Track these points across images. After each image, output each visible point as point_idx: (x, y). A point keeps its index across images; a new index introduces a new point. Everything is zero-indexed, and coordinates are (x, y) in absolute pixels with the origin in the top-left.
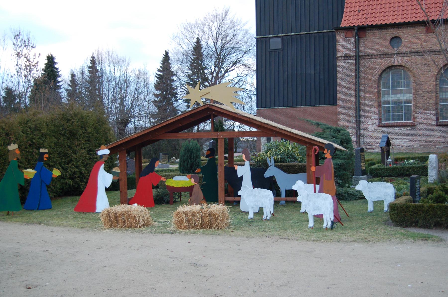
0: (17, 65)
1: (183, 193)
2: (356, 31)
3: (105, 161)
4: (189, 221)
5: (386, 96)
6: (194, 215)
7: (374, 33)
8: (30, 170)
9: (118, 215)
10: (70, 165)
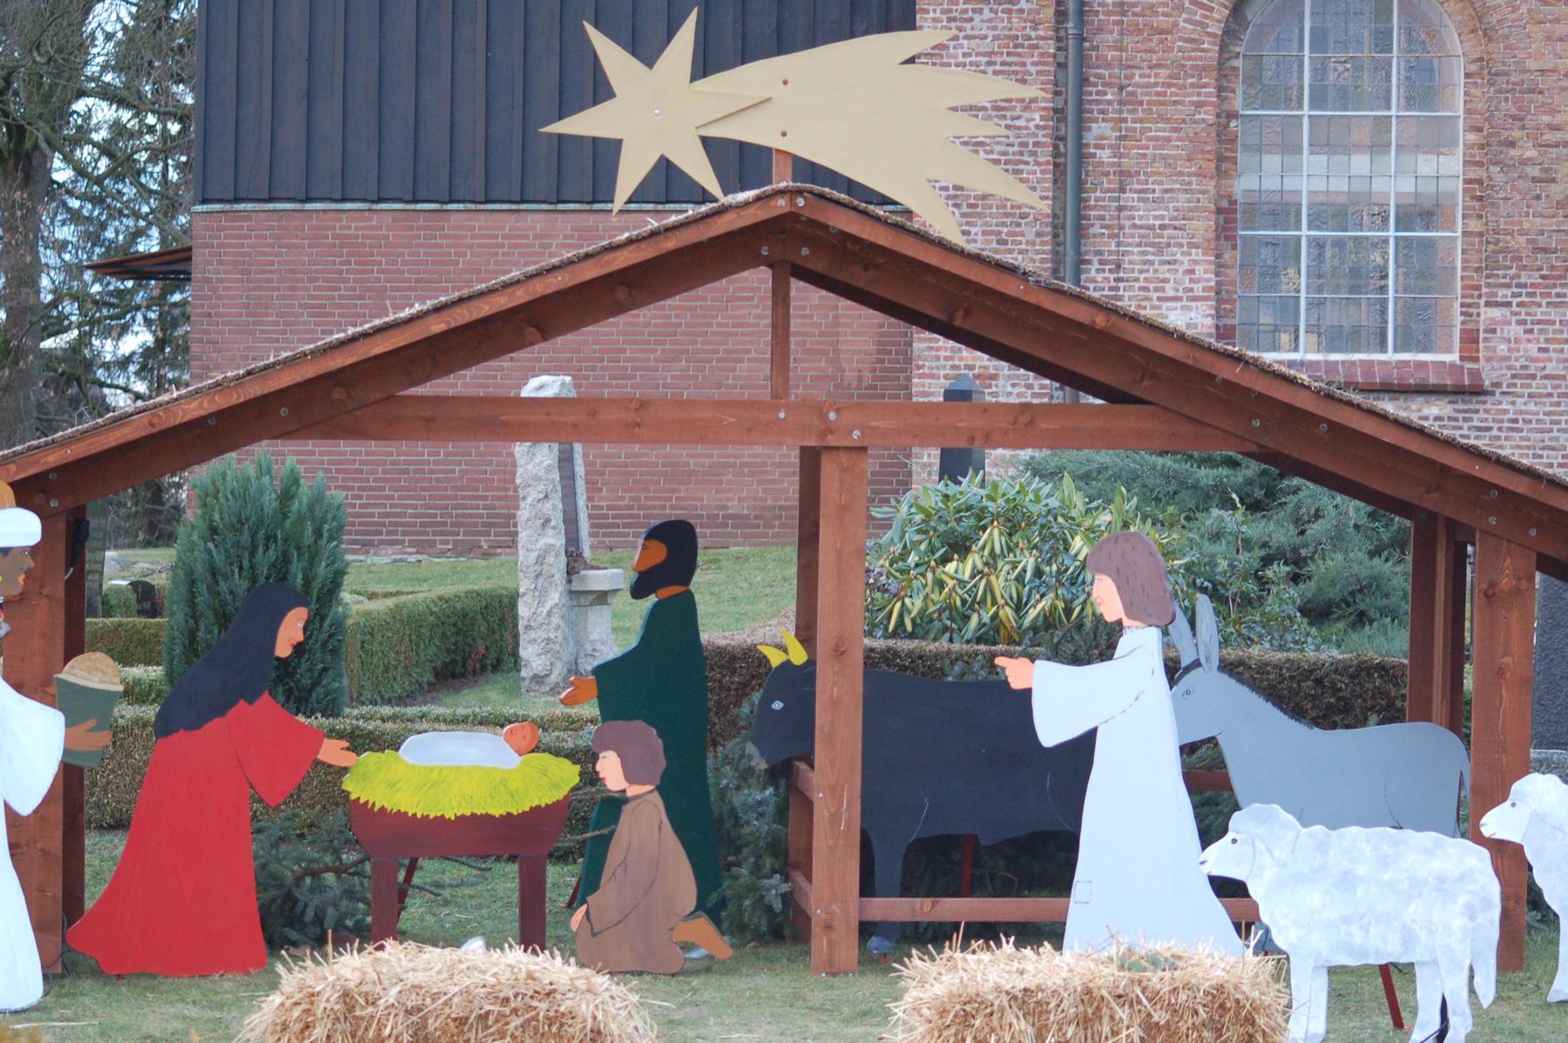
5: (1272, 161)
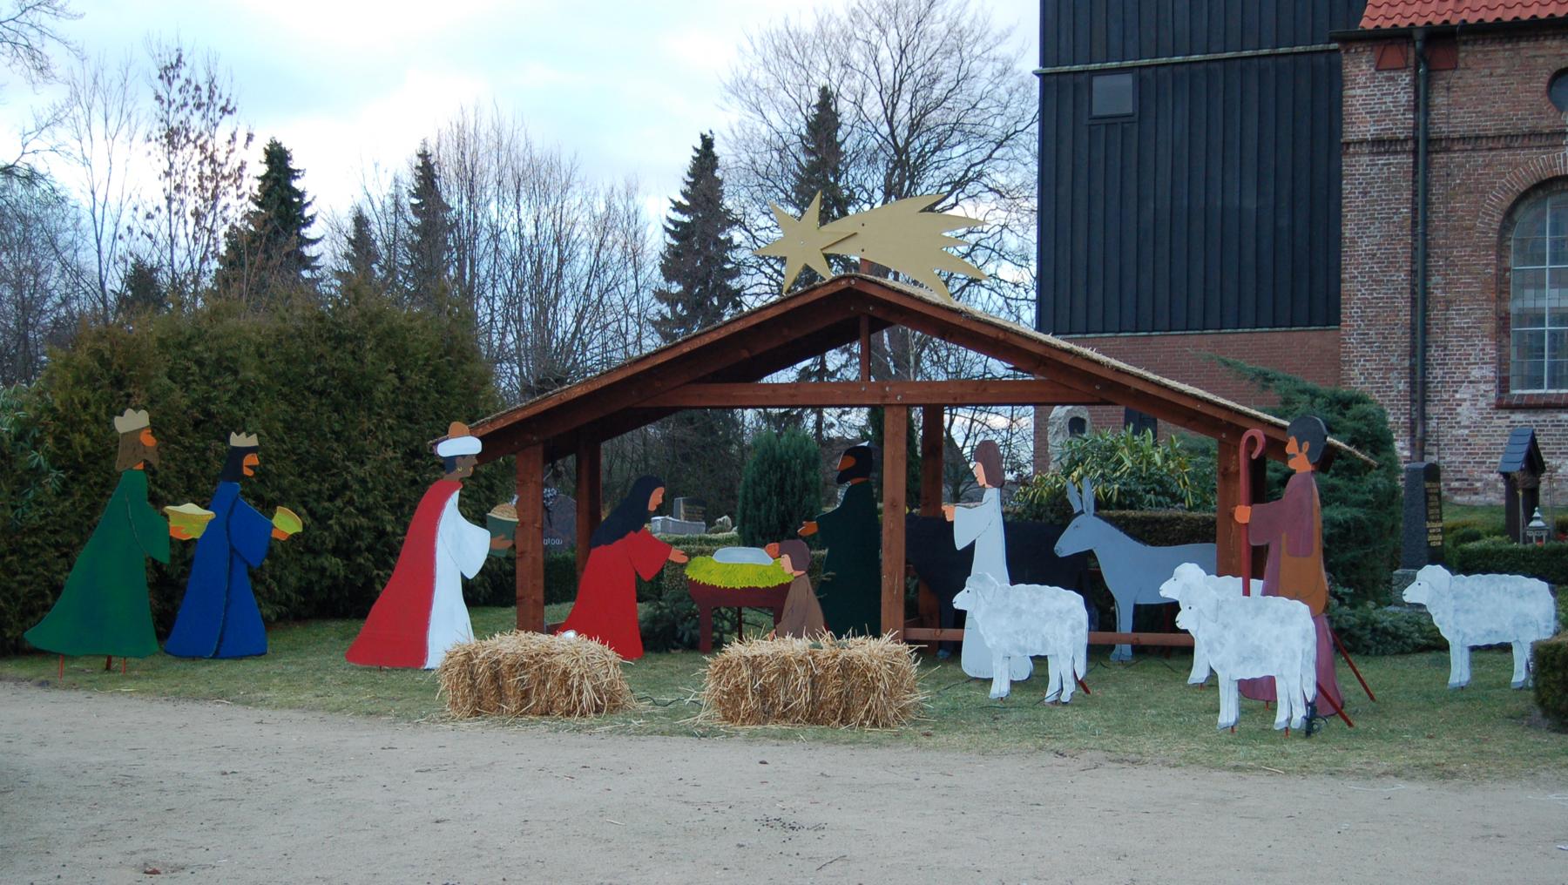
0: (168, 174)
1: (749, 615)
2: (1418, 45)
3: (462, 481)
4: (764, 693)
5: (1530, 293)
6: (784, 673)
7: (1486, 53)
8: (190, 508)
9: (504, 668)
10: (339, 503)
